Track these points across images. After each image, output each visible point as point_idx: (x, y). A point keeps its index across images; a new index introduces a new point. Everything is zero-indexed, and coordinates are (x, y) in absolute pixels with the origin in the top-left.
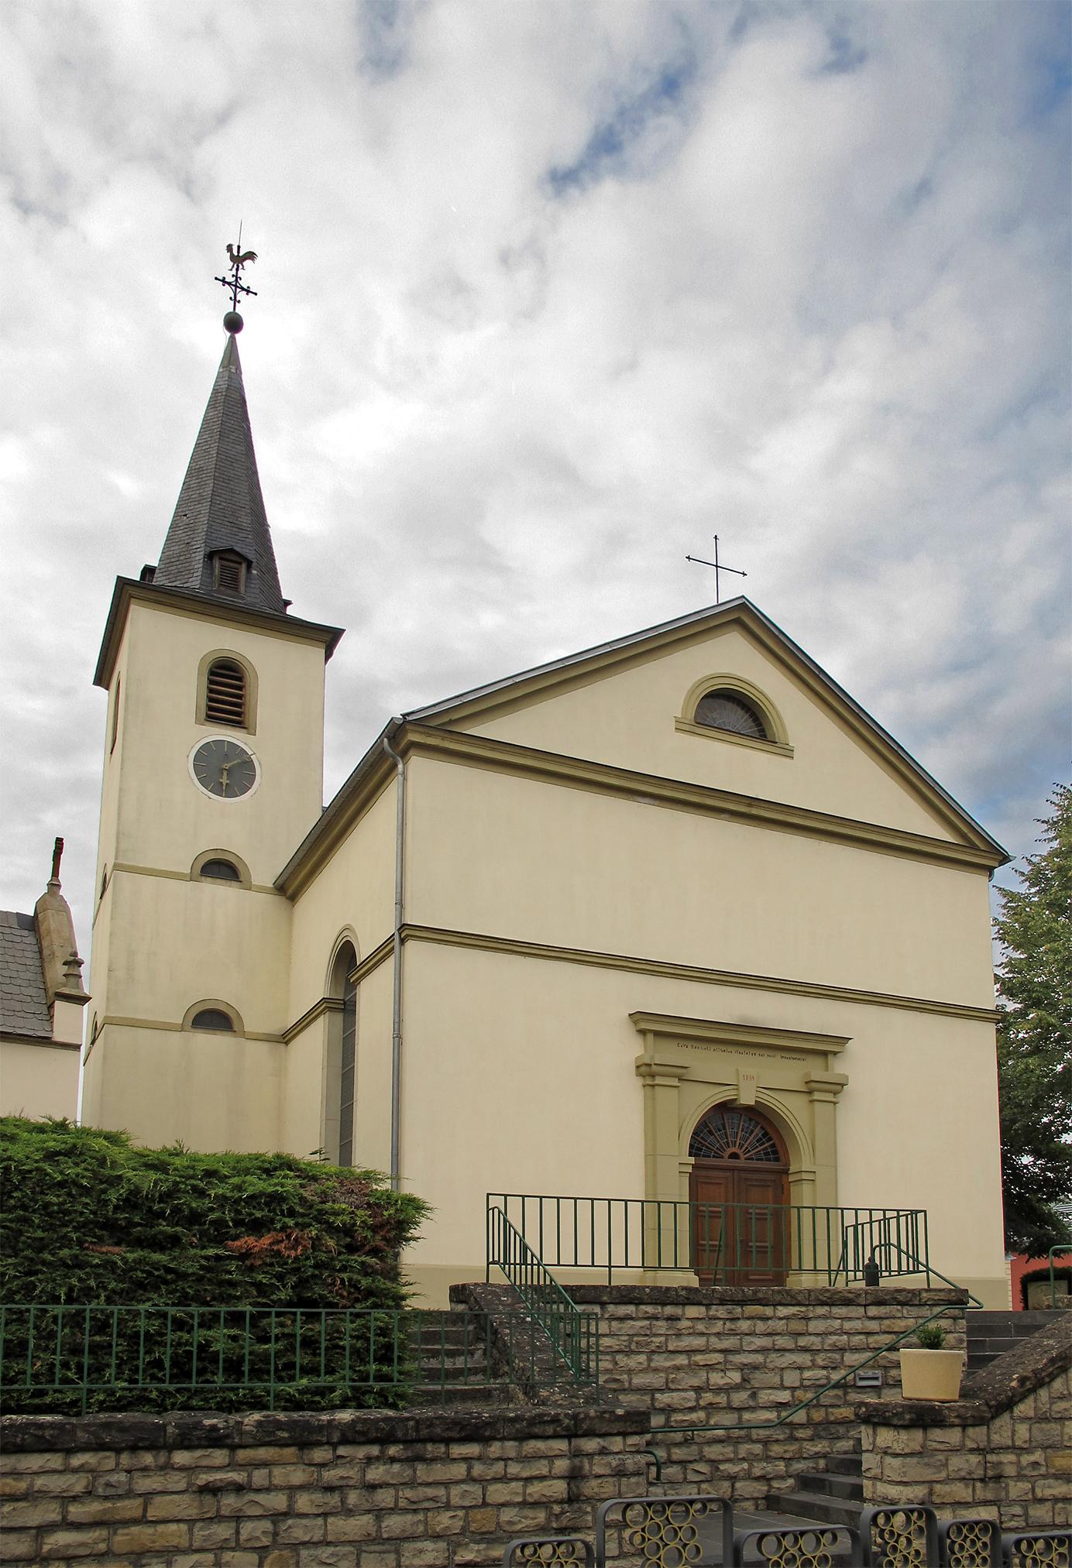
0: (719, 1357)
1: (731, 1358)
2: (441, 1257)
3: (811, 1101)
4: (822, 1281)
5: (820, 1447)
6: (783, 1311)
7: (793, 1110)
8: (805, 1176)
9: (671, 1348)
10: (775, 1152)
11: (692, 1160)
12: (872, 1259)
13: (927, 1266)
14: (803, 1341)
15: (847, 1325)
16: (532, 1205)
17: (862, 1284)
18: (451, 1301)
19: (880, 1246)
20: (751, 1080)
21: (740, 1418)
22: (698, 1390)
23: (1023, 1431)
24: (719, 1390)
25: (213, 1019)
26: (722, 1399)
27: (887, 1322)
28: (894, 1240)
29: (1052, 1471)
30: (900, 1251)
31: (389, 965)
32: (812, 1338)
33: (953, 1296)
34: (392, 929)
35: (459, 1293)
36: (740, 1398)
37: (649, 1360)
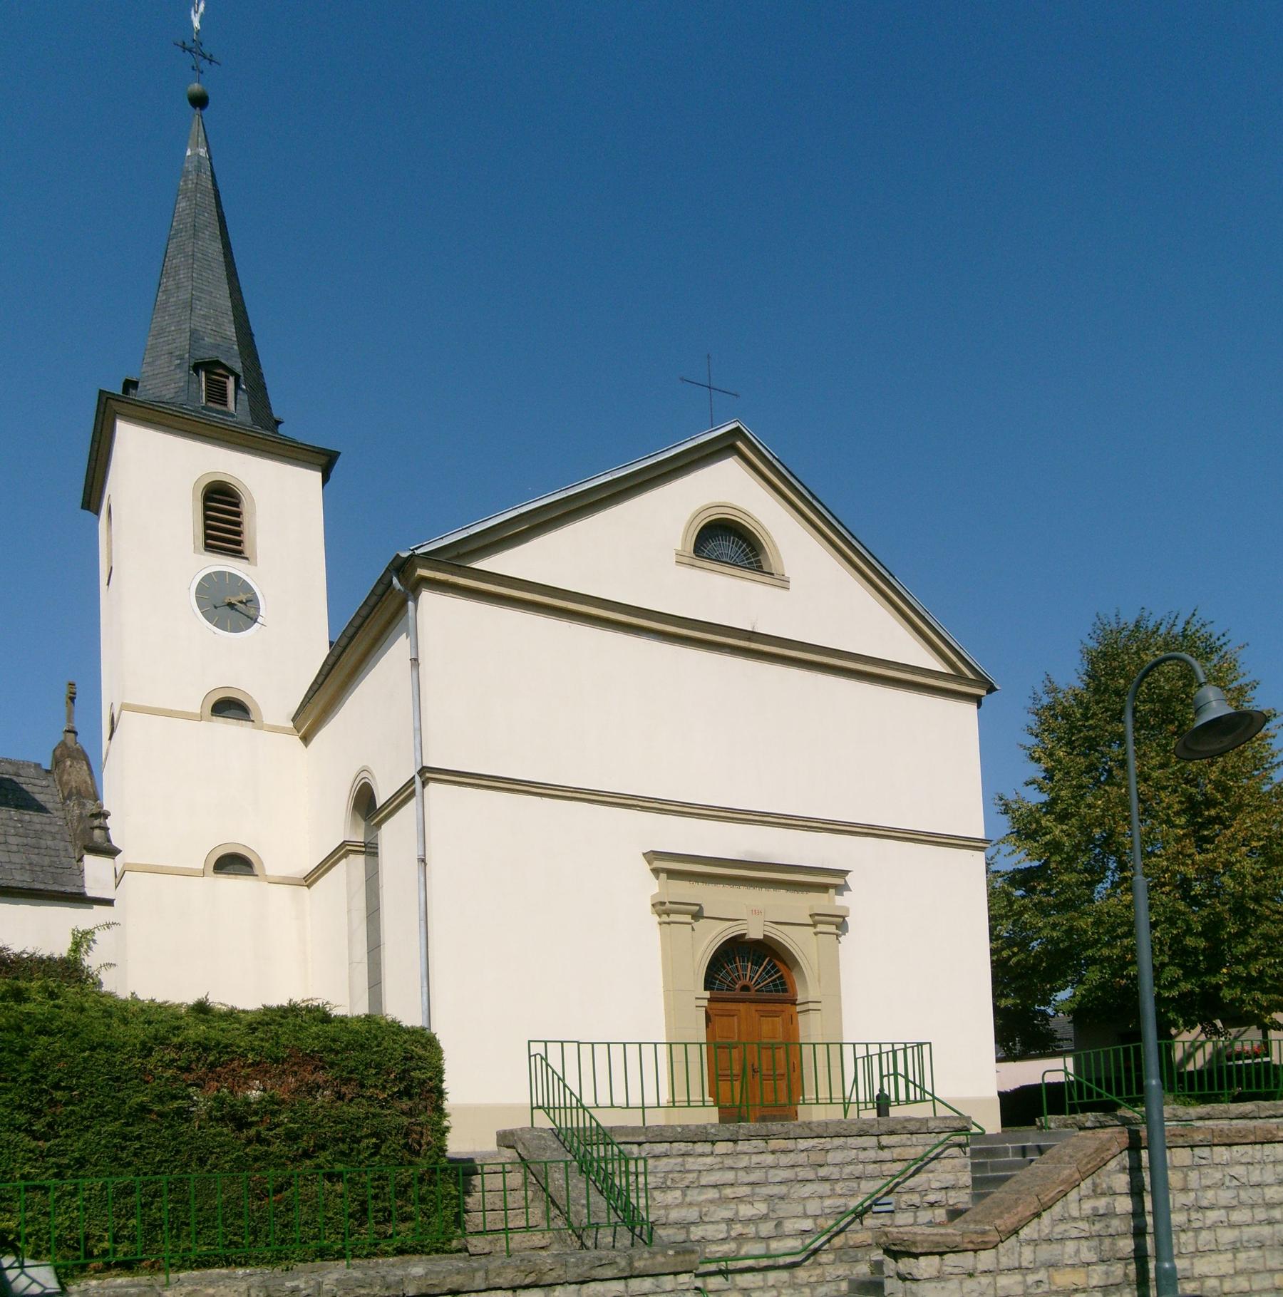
0: (745, 1190)
1: (758, 1190)
2: (482, 1098)
3: (816, 934)
4: (835, 1113)
5: (842, 1270)
6: (803, 1144)
7: (799, 942)
8: (811, 1006)
9: (703, 1182)
10: (783, 984)
11: (707, 994)
12: (882, 1090)
13: (932, 1095)
14: (823, 1172)
15: (862, 1155)
16: (571, 1049)
17: (873, 1114)
18: (499, 1145)
19: (888, 1075)
20: (754, 913)
21: (768, 1247)
22: (730, 1221)
23: (1027, 1253)
24: (749, 1221)
25: (233, 863)
26: (751, 1230)
27: (897, 1150)
28: (901, 1070)
29: (1054, 1288)
30: (907, 1081)
31: (411, 808)
32: (831, 1168)
33: (957, 1124)
34: (412, 771)
35: (506, 1139)
36: (766, 1229)
37: (684, 1195)
